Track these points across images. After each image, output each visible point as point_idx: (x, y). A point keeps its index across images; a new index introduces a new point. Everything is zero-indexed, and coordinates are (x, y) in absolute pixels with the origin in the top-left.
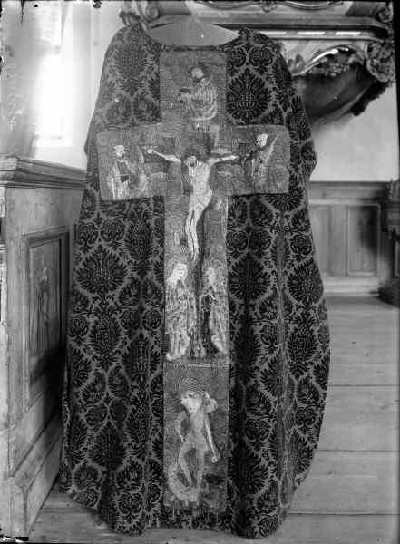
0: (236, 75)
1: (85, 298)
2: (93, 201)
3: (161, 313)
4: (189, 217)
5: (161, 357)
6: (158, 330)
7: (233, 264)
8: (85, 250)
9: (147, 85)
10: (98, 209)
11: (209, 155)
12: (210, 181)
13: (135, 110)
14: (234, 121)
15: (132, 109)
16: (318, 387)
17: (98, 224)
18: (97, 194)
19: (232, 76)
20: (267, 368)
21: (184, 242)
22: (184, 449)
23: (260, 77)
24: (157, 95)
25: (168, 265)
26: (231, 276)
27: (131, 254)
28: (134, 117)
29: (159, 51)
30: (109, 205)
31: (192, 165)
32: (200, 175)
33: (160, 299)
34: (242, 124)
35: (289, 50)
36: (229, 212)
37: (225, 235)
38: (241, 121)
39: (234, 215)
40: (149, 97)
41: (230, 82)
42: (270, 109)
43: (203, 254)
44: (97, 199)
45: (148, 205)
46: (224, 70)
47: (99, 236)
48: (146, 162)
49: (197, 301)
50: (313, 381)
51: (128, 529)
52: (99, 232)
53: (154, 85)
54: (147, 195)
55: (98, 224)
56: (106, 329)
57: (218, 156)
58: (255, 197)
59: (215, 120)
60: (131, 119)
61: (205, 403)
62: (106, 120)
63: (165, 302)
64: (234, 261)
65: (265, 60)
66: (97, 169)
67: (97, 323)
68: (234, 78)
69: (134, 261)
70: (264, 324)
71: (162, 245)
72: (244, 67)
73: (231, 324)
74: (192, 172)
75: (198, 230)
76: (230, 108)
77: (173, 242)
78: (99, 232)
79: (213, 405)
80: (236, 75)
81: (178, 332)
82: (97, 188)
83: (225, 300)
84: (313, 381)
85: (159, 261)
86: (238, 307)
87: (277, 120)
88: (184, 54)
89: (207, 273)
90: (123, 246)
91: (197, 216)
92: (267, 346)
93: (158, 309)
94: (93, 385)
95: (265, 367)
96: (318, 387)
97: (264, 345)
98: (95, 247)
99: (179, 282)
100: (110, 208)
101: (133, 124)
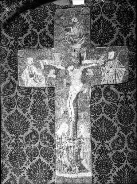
0: (96, 19)
1: (6, 38)
2: (14, 86)
3: (53, 150)
4: (69, 99)
5: (54, 173)
6: (52, 158)
7: (94, 122)
8: (9, 111)
9: (47, 27)
10: (16, 90)
12: (81, 79)
13: (40, 40)
14: (95, 45)
15: (38, 39)
17: (16, 98)
18: (16, 82)
19: (93, 20)
20: (116, 175)
21: (66, 112)
23: (109, 20)
24: (52, 33)
25: (57, 124)
26: (92, 129)
27: (33, 117)
28: (39, 43)
29: (55, 9)
30: (22, 89)
31: (72, 71)
32: (76, 74)
33: (53, 143)
34: (98, 46)
36: (91, 94)
37: (89, 107)
38: (98, 45)
39: (94, 96)
40: (49, 132)
41: (92, 23)
43: (77, 118)
44: (17, 85)
45: (45, 91)
46: (89, 17)
47: (17, 105)
48: (44, 69)
52: (16, 102)
53: (51, 28)
54: (44, 86)
56: (17, 154)
58: (107, 86)
59: (84, 45)
60: (37, 44)
62: (23, 44)
63: (55, 145)
64: (94, 121)
65: (111, 10)
66: (17, 69)
67: (13, 150)
68: (95, 21)
69: (34, 120)
70: (114, 152)
71: (54, 113)
72: (100, 15)
73: (92, 155)
74: (71, 74)
76: (93, 38)
77: (60, 113)
78: (16, 102)
80: (96, 19)
81: (63, 159)
82: (17, 79)
83: (89, 142)
86: (96, 145)
88: (67, 9)
89: (80, 128)
90: (29, 112)
91: (74, 97)
92: (116, 164)
93: (52, 148)
94: (8, 84)
95: (115, 174)
97: (114, 163)
98: (14, 110)
99: (63, 134)
100: (23, 91)
101: (39, 47)
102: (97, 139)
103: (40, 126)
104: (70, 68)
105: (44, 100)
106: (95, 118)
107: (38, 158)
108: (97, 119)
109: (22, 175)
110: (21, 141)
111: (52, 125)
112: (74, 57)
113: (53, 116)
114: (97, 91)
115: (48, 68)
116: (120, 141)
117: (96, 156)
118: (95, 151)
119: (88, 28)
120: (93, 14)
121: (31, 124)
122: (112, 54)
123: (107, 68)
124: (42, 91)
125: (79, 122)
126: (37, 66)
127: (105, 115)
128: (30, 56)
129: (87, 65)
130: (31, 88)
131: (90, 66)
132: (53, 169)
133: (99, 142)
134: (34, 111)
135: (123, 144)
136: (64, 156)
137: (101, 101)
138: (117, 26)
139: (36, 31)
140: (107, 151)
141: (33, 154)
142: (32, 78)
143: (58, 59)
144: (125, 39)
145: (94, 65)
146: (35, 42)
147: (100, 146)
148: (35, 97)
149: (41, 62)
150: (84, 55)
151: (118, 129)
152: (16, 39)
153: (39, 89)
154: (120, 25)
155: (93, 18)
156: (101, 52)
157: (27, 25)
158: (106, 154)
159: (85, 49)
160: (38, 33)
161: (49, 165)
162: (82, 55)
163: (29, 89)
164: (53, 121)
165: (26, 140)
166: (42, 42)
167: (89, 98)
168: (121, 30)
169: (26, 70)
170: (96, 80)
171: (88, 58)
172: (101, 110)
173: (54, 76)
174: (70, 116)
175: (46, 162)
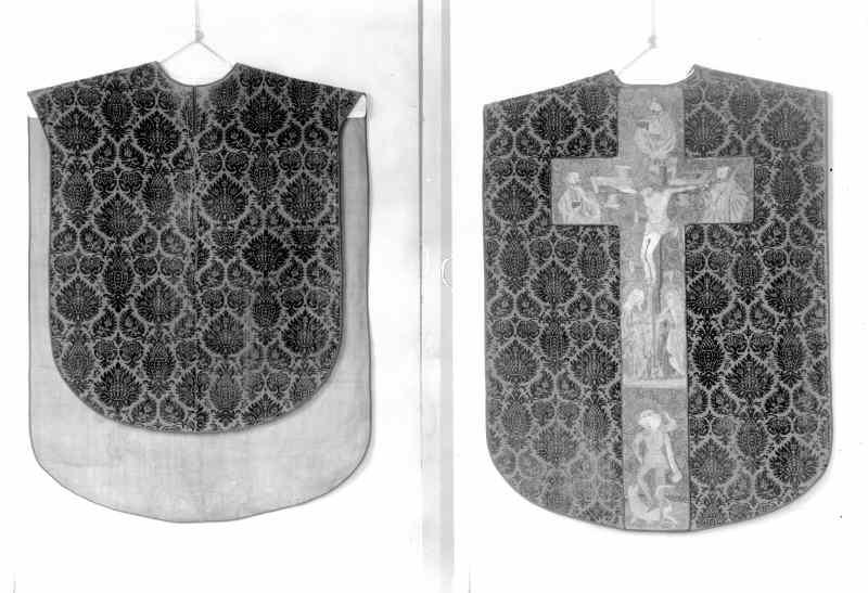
7: (690, 283)
11: (665, 183)
14: (691, 154)
16: (811, 227)
17: (554, 242)
21: (639, 269)
22: (643, 471)
35: (726, 168)
40: (610, 297)
42: (727, 141)
43: (661, 280)
47: (553, 253)
49: (654, 325)
50: (805, 222)
51: (580, 513)
55: (554, 242)
57: (674, 187)
59: (674, 154)
61: (665, 422)
64: (691, 281)
74: (648, 202)
75: (655, 259)
79: (672, 425)
84: (805, 222)
85: (615, 280)
87: (734, 151)
96: (811, 227)
98: (549, 262)
99: (636, 307)
102: (696, 312)
103: (594, 288)
104: (644, 193)
105: (601, 245)
106: (693, 276)
107: (590, 342)
108: (697, 278)
109: (563, 371)
110: (561, 314)
111: (615, 287)
112: (653, 173)
113: (619, 431)
114: (695, 234)
115: (605, 192)
116: (738, 315)
117: (696, 340)
118: (693, 332)
119: (679, 123)
120: (689, 102)
121: (579, 286)
122: (723, 171)
123: (714, 193)
124: (598, 230)
125: (665, 287)
126: (587, 187)
127: (710, 271)
128: (571, 171)
129: (678, 187)
130: (578, 227)
131: (681, 190)
132: (617, 360)
133: (701, 316)
134: (583, 264)
135: (742, 320)
136: (637, 349)
137: (702, 248)
138: (731, 122)
139: (589, 130)
140: (714, 331)
141: (582, 336)
142: (576, 209)
143: (623, 176)
144: (744, 144)
145: (690, 188)
146: (152, 414)
147: (702, 323)
148: (585, 240)
149: (593, 179)
150: (672, 170)
151: (734, 294)
152: (553, 144)
153: (593, 226)
154: (735, 120)
155: (688, 109)
156: (703, 166)
157: (573, 120)
158: (713, 338)
159: (675, 160)
160: (593, 135)
161: (611, 354)
162: (669, 170)
163: (576, 228)
164: (618, 278)
165: (571, 312)
166: (600, 148)
167: (682, 246)
168: (738, 127)
169: (567, 195)
170: (695, 214)
171: (680, 176)
172: (704, 263)
173: (616, 206)
174: (648, 275)
175: (605, 348)
